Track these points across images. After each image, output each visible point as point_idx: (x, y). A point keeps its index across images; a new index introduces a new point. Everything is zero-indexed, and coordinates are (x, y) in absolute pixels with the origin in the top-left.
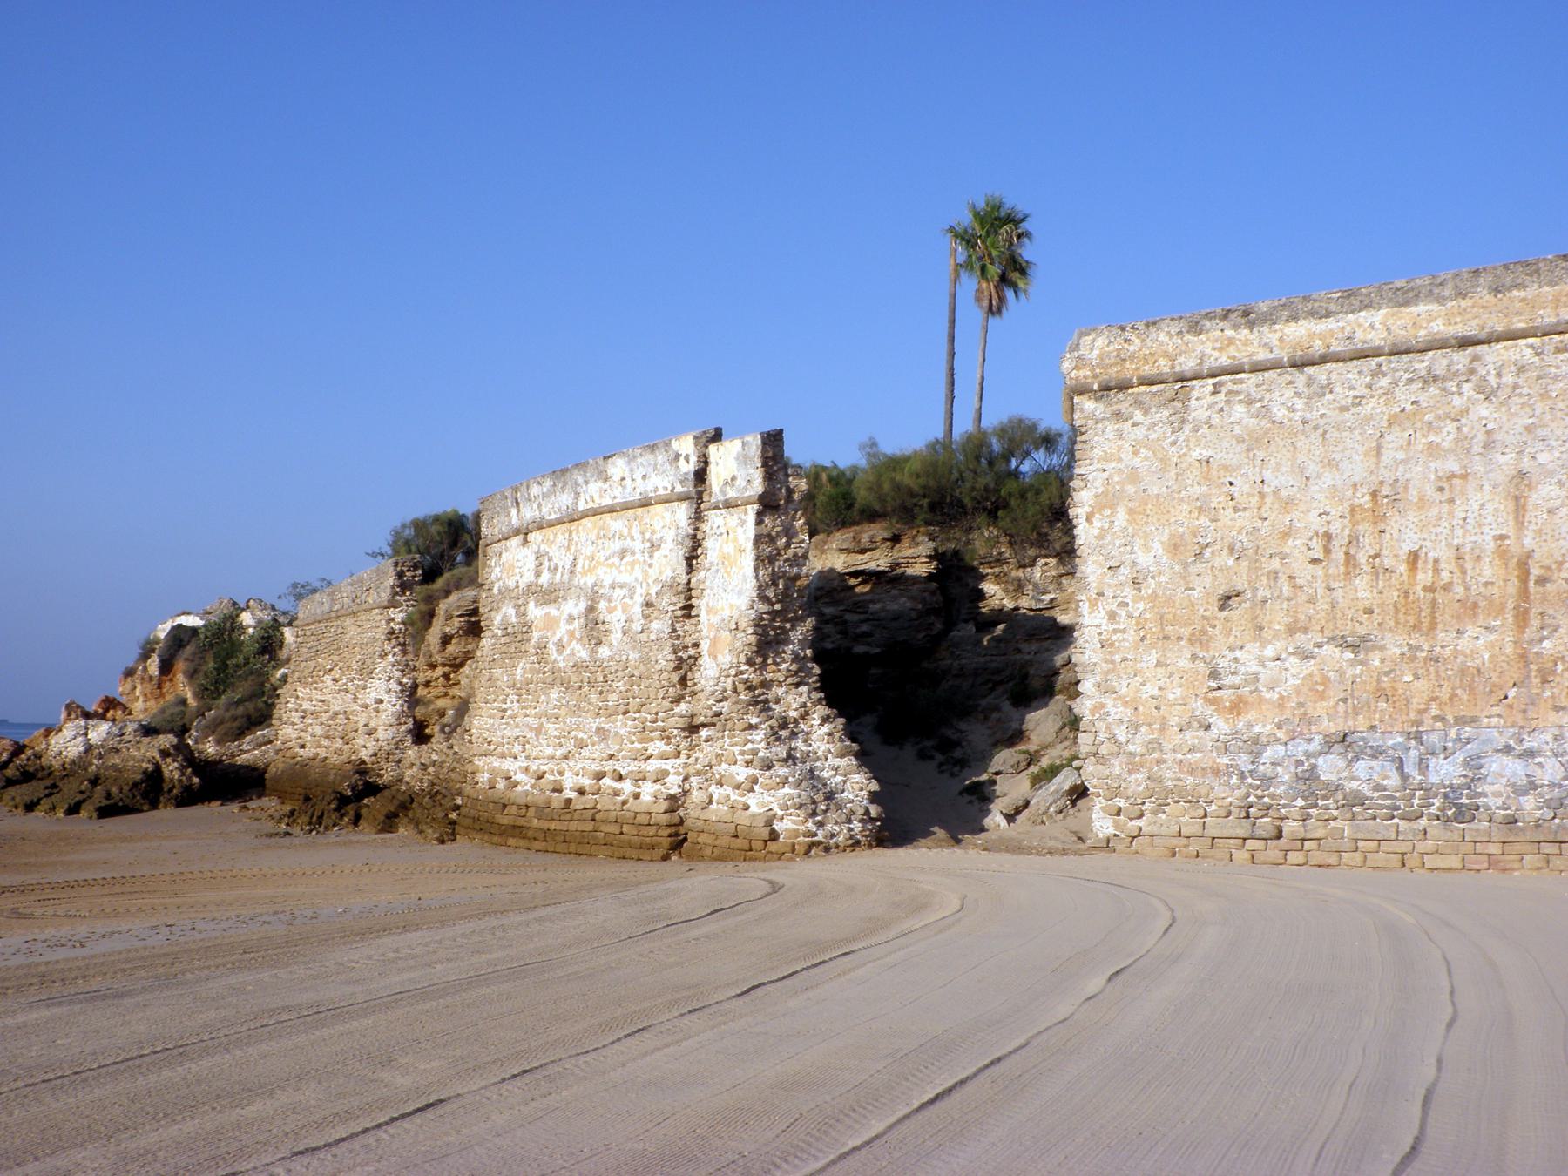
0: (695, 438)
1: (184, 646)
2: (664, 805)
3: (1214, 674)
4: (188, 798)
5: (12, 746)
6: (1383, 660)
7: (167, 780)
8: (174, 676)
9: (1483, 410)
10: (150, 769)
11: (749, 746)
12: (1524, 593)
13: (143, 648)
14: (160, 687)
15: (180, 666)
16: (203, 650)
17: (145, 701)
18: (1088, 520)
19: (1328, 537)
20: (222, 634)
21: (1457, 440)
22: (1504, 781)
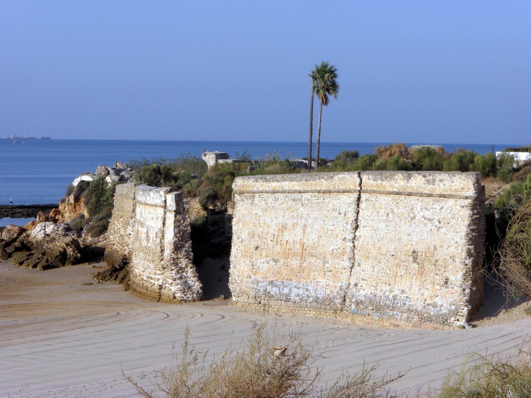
0: (164, 192)
1: (84, 190)
2: (158, 287)
3: (253, 265)
4: (76, 262)
5: (18, 230)
6: (280, 265)
7: (68, 255)
8: (80, 203)
9: (301, 209)
10: (62, 251)
11: (172, 275)
12: (302, 252)
13: (68, 191)
14: (75, 207)
15: (83, 199)
16: (91, 193)
17: (70, 213)
18: (235, 225)
19: (274, 235)
20: (99, 186)
21: (297, 215)
22: (294, 294)
